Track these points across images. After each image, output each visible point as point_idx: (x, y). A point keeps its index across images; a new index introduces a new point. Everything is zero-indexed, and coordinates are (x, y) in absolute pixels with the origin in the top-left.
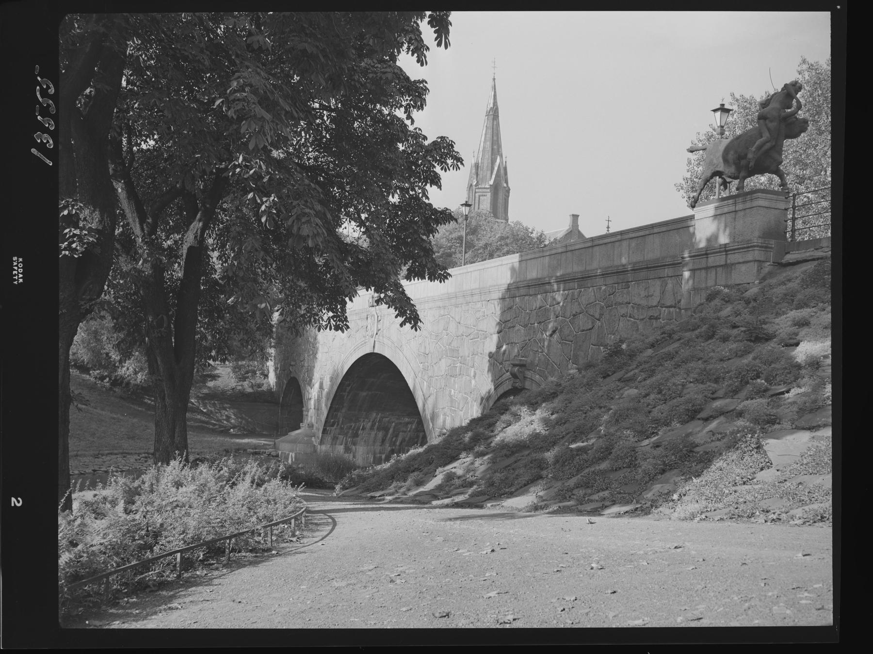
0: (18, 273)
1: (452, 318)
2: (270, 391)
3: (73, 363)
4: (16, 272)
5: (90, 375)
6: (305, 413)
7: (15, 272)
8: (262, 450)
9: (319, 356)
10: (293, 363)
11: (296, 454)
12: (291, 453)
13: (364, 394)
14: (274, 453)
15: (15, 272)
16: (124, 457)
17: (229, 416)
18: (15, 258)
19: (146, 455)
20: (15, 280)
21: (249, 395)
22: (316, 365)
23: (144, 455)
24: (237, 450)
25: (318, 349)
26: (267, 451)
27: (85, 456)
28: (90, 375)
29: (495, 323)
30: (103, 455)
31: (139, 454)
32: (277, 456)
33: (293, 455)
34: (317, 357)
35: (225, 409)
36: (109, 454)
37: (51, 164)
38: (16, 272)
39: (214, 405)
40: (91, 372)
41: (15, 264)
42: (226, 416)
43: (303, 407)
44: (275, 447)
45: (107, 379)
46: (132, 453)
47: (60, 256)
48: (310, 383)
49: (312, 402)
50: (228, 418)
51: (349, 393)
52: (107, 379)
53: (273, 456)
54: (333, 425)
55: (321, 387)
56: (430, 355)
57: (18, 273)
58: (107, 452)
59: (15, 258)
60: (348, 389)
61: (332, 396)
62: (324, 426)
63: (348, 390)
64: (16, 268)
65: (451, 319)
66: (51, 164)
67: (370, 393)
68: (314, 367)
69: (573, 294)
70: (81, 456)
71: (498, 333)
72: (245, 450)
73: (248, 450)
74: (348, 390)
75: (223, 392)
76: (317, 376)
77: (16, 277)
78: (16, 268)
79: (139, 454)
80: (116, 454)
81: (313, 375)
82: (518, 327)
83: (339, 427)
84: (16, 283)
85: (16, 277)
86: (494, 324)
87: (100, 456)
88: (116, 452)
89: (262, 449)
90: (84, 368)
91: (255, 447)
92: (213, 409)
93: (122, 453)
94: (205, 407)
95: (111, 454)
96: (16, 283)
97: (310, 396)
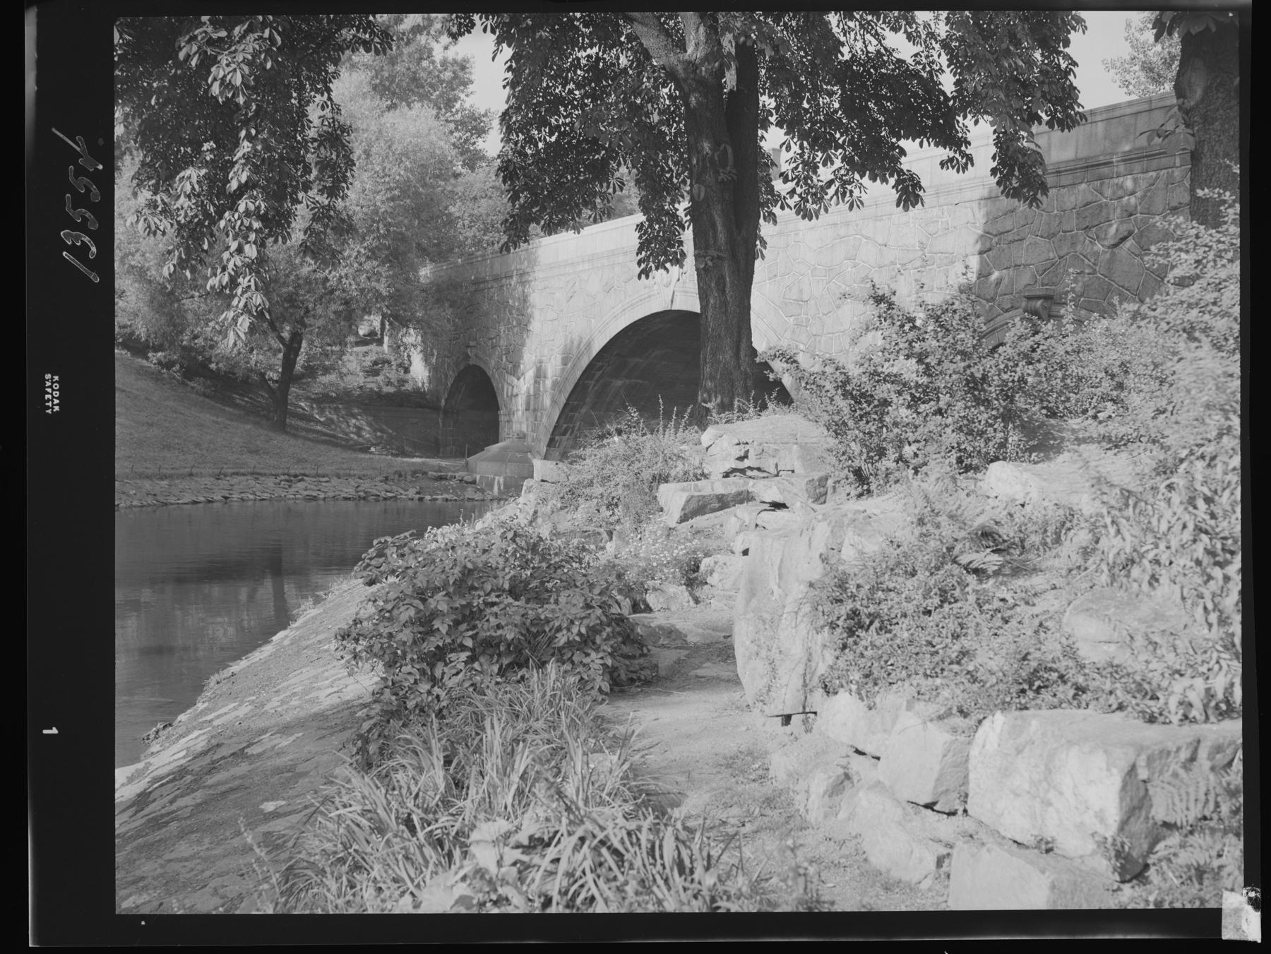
0: (53, 397)
1: (867, 238)
2: (417, 392)
3: (121, 340)
4: (50, 396)
5: (147, 358)
6: (502, 419)
7: (47, 396)
8: (450, 474)
9: (535, 326)
10: (472, 343)
11: (505, 478)
12: (497, 478)
13: (619, 383)
14: (468, 478)
15: (47, 396)
16: (257, 479)
17: (360, 426)
18: (48, 376)
19: (287, 477)
20: (48, 408)
21: (388, 396)
22: (528, 341)
23: (283, 477)
24: (414, 473)
25: (531, 316)
26: (457, 475)
27: (201, 475)
28: (147, 358)
29: (976, 237)
30: (226, 475)
31: (276, 476)
32: (474, 482)
33: (502, 480)
34: (531, 328)
35: (354, 416)
36: (234, 474)
37: (64, 253)
38: (50, 396)
39: (336, 410)
40: (150, 355)
41: (48, 384)
42: (355, 426)
43: (498, 409)
44: (467, 467)
45: (178, 367)
46: (265, 475)
47: (45, 732)
48: (515, 370)
49: (520, 403)
50: (359, 430)
51: (597, 381)
52: (178, 367)
53: (467, 482)
54: (564, 434)
55: (540, 375)
56: (812, 302)
57: (53, 397)
58: (230, 471)
59: (48, 376)
60: (598, 374)
61: (570, 388)
62: (552, 434)
63: (596, 378)
64: (49, 390)
65: (864, 240)
66: (64, 253)
67: (628, 381)
68: (523, 345)
69: (1170, 176)
70: (196, 475)
71: (981, 253)
72: (425, 473)
73: (430, 473)
74: (596, 378)
75: (347, 393)
76: (528, 360)
77: (50, 404)
78: (49, 390)
79: (276, 476)
80: (244, 475)
81: (521, 357)
82: (1030, 239)
83: (574, 435)
84: (49, 411)
85: (50, 404)
86: (972, 239)
87: (222, 476)
88: (242, 471)
89: (450, 471)
90: (139, 348)
91: (440, 469)
92: (335, 417)
93: (252, 474)
94: (322, 412)
95: (237, 474)
96: (49, 411)
97: (515, 391)
